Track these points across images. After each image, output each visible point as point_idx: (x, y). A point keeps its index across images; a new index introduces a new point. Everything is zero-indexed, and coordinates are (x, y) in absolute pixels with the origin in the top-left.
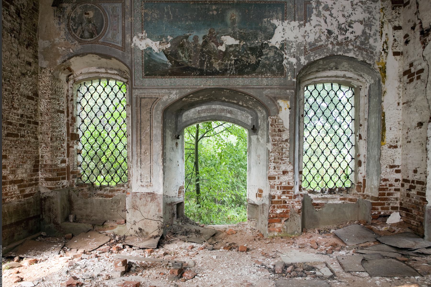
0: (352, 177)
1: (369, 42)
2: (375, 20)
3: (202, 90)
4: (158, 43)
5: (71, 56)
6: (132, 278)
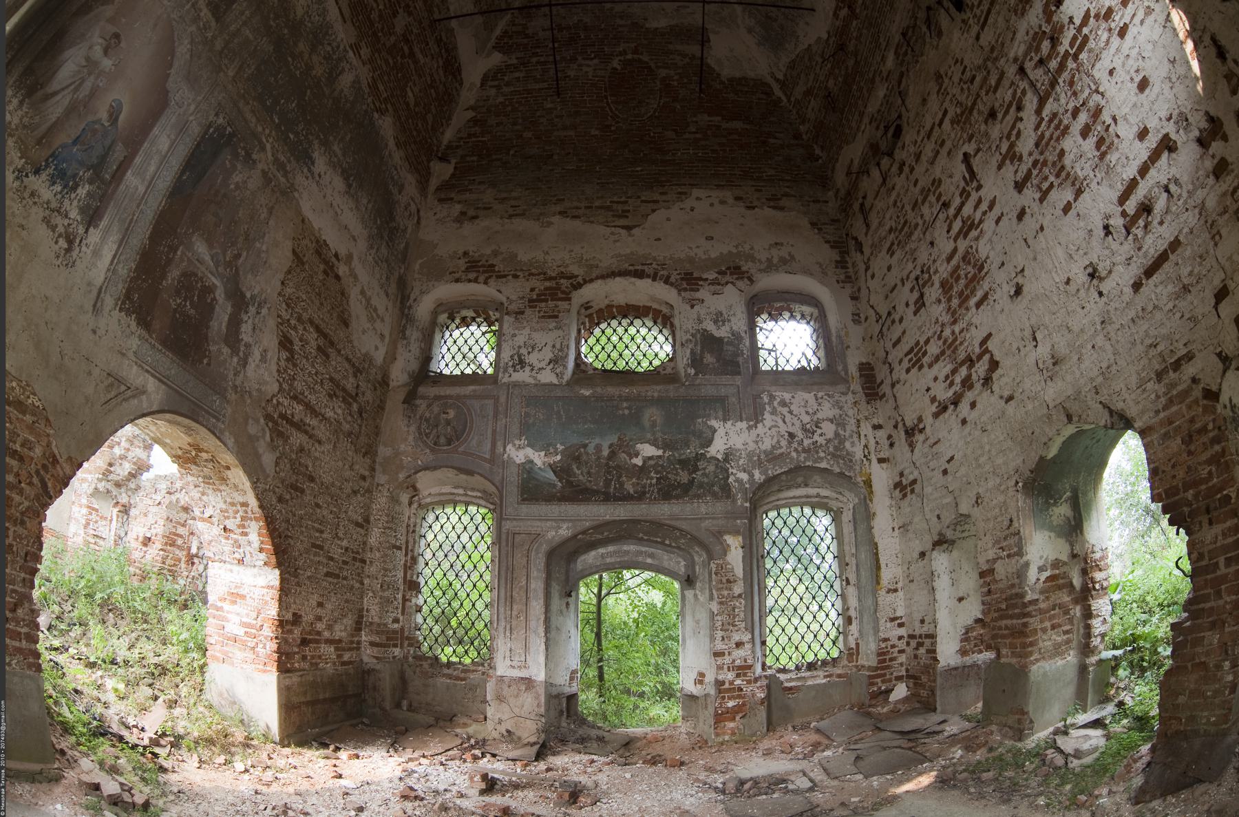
0: (840, 643)
3: (607, 523)
4: (543, 453)
6: (497, 800)
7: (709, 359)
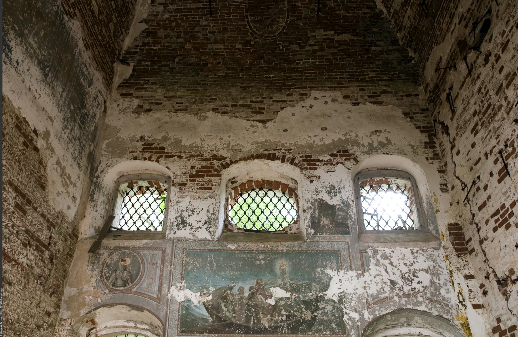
1: (440, 293)
2: (442, 268)
5: (98, 306)
7: (325, 222)
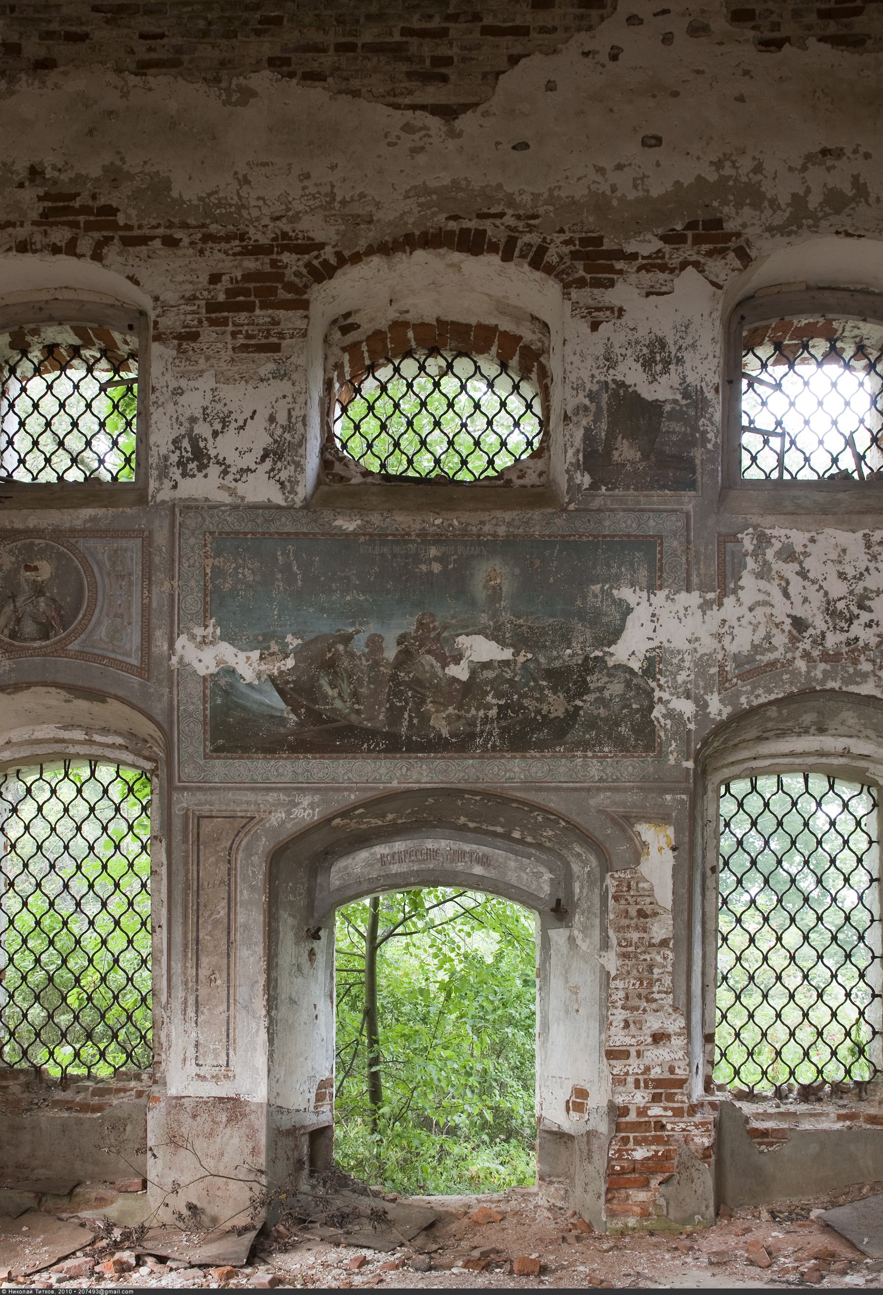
4: (255, 655)
